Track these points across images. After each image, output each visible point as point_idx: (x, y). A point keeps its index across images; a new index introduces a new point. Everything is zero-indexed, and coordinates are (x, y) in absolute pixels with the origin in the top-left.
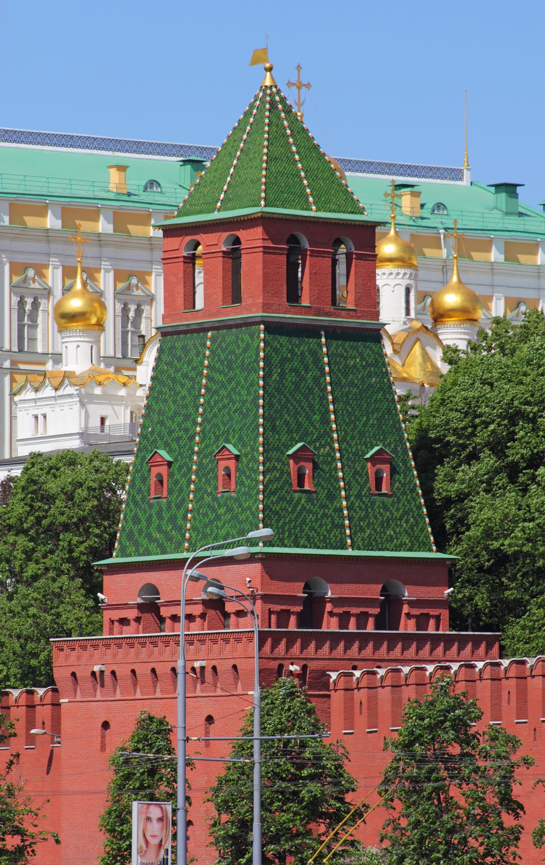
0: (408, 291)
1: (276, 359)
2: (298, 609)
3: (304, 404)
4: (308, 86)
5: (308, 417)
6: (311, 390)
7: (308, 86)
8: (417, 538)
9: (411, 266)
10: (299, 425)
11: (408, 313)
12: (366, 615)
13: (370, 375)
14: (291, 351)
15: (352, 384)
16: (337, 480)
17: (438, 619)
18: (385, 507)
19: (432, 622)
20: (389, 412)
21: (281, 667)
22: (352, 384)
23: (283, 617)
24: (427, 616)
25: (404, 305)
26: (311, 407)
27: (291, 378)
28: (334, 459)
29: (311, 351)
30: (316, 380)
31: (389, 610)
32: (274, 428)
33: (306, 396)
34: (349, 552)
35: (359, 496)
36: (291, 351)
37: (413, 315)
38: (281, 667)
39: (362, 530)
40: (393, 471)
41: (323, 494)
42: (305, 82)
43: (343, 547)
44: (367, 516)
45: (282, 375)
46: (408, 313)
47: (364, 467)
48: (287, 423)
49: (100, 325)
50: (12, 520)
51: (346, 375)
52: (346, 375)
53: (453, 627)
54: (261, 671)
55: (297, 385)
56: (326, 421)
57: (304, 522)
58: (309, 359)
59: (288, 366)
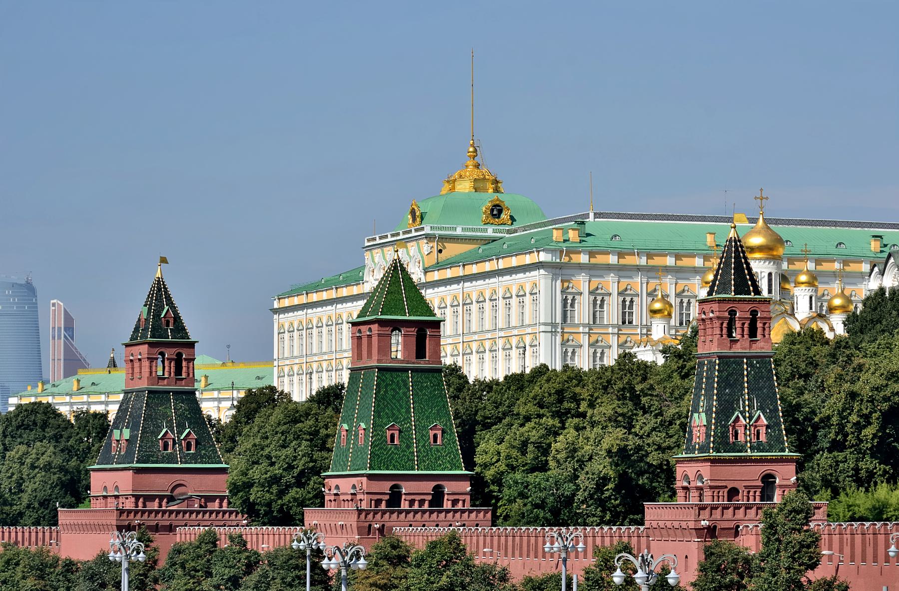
0: (811, 298)
1: (383, 384)
2: (387, 497)
3: (398, 405)
4: (767, 198)
5: (399, 411)
6: (401, 398)
7: (767, 198)
8: (455, 465)
9: (814, 286)
10: (393, 414)
11: (811, 308)
12: (424, 500)
13: (435, 390)
14: (392, 381)
15: (425, 395)
16: (412, 439)
17: (464, 501)
18: (438, 451)
19: (461, 502)
20: (444, 406)
21: (370, 526)
22: (425, 395)
23: (378, 502)
24: (458, 500)
25: (808, 305)
26: (401, 406)
27: (391, 393)
28: (411, 429)
29: (402, 380)
30: (405, 394)
31: (437, 497)
32: (379, 416)
33: (398, 401)
34: (416, 472)
35: (424, 446)
36: (392, 381)
37: (814, 309)
38: (370, 526)
39: (424, 461)
40: (443, 432)
41: (404, 446)
42: (764, 196)
43: (413, 469)
44: (427, 455)
45: (386, 392)
46: (811, 308)
47: (427, 432)
48: (387, 414)
49: (670, 315)
50: (29, 486)
51: (421, 391)
52: (421, 391)
53: (471, 506)
54: (358, 528)
55: (394, 396)
56: (408, 412)
57: (392, 458)
58: (401, 384)
59: (389, 388)
